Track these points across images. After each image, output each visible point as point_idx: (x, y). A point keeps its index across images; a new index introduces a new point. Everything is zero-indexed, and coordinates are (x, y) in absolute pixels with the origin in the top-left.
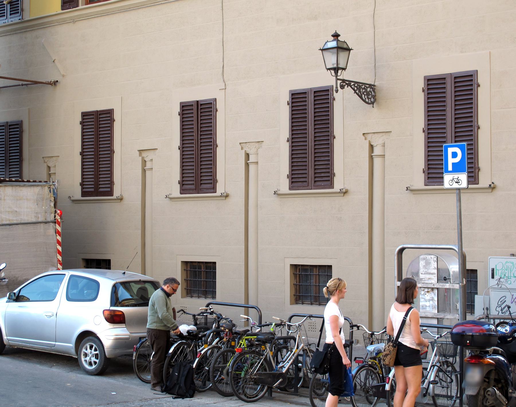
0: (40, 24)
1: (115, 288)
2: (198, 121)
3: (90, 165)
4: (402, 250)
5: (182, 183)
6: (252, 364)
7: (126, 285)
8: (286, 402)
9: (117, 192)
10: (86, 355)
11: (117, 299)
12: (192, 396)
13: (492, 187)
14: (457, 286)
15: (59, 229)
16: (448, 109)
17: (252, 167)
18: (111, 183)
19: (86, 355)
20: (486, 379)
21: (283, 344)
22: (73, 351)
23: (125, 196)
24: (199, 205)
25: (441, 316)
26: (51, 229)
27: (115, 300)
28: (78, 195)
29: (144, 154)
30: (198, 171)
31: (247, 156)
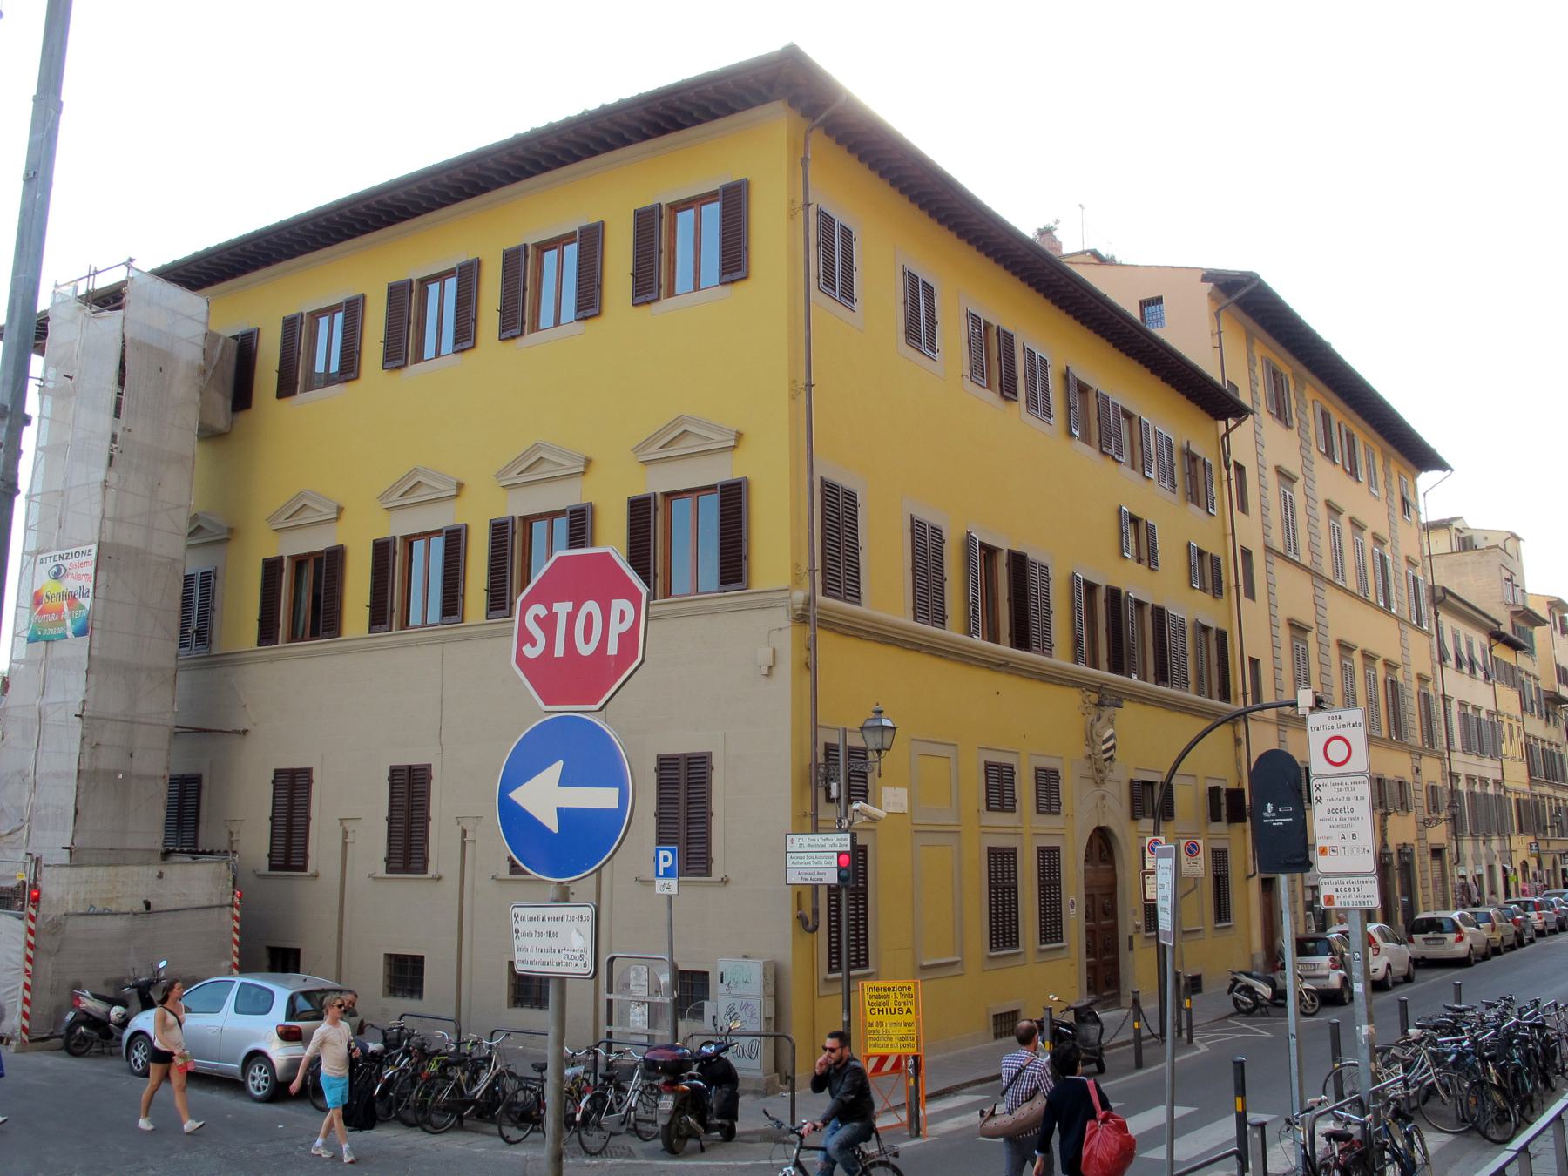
0: (231, 660)
1: (292, 999)
2: (409, 789)
3: (282, 832)
4: (612, 960)
5: (388, 860)
6: (440, 1091)
7: (307, 995)
8: (477, 1132)
9: (311, 868)
10: (254, 1078)
11: (294, 1010)
12: (371, 1128)
13: (725, 881)
14: (667, 1000)
15: (237, 913)
16: (682, 792)
17: (469, 846)
18: (305, 856)
19: (254, 1078)
20: (678, 1110)
21: (476, 1067)
22: (239, 1073)
23: (321, 873)
24: (406, 887)
25: (651, 1032)
26: (226, 915)
27: (292, 1013)
28: (264, 866)
29: (346, 824)
30: (407, 848)
31: (464, 833)
